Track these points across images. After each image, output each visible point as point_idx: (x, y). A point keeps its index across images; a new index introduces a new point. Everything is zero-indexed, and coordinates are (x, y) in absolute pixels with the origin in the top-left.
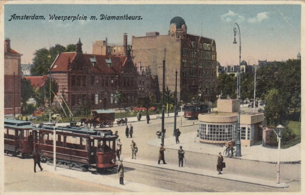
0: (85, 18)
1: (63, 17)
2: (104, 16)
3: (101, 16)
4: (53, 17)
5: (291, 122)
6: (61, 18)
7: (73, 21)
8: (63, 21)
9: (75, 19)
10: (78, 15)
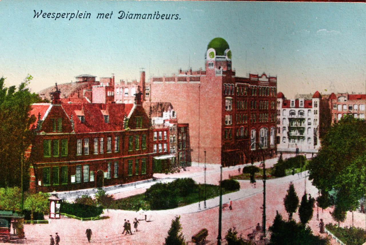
0: (89, 15)
2: (124, 14)
3: (119, 13)
4: (39, 14)
6: (52, 16)
9: (72, 18)
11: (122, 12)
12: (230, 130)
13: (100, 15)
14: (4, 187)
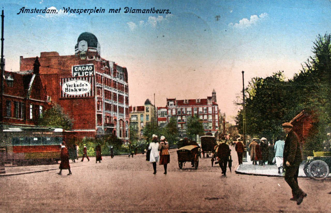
0: (103, 11)
1: (79, 10)
2: (128, 9)
3: (125, 9)
5: (221, 169)
6: (77, 11)
7: (89, 14)
8: (79, 14)
9: (92, 12)
10: (96, 8)
11: (127, 8)
12: (122, 81)
13: (111, 10)
14: (246, 17)
